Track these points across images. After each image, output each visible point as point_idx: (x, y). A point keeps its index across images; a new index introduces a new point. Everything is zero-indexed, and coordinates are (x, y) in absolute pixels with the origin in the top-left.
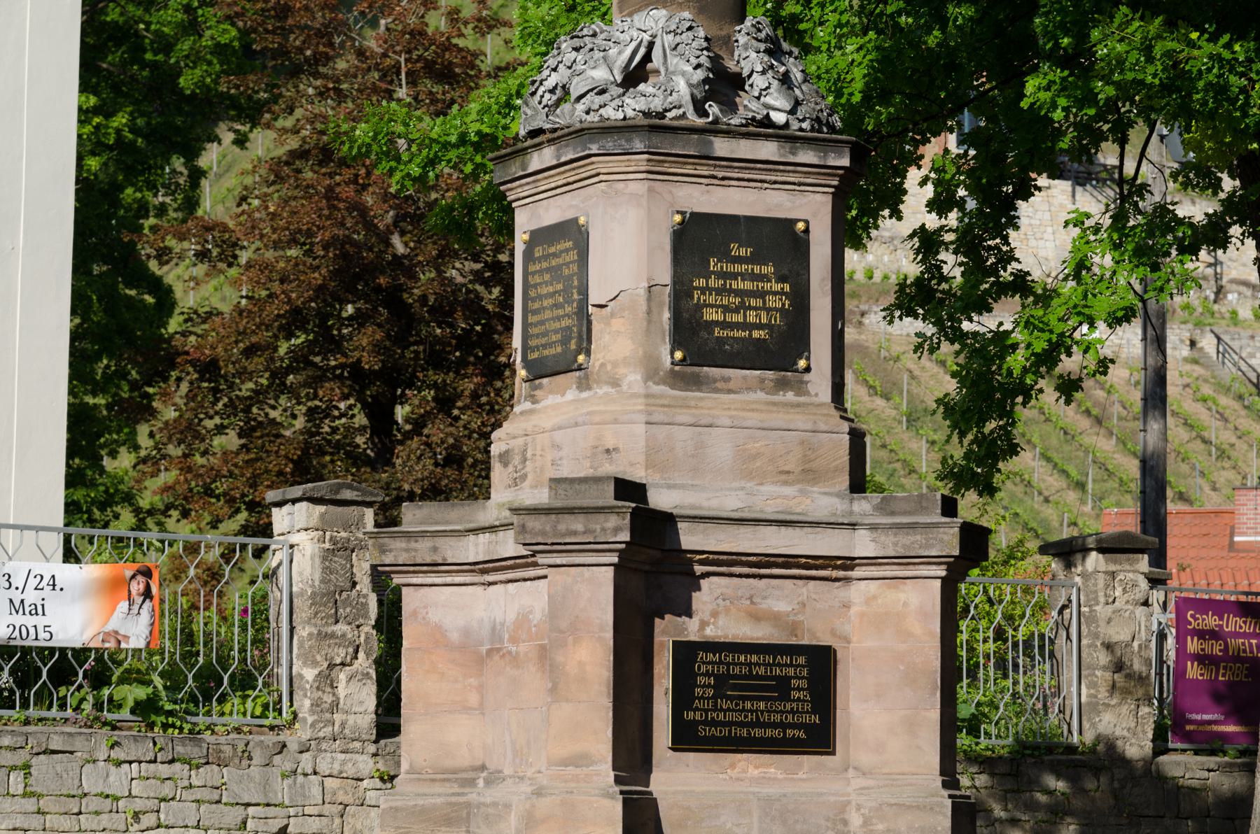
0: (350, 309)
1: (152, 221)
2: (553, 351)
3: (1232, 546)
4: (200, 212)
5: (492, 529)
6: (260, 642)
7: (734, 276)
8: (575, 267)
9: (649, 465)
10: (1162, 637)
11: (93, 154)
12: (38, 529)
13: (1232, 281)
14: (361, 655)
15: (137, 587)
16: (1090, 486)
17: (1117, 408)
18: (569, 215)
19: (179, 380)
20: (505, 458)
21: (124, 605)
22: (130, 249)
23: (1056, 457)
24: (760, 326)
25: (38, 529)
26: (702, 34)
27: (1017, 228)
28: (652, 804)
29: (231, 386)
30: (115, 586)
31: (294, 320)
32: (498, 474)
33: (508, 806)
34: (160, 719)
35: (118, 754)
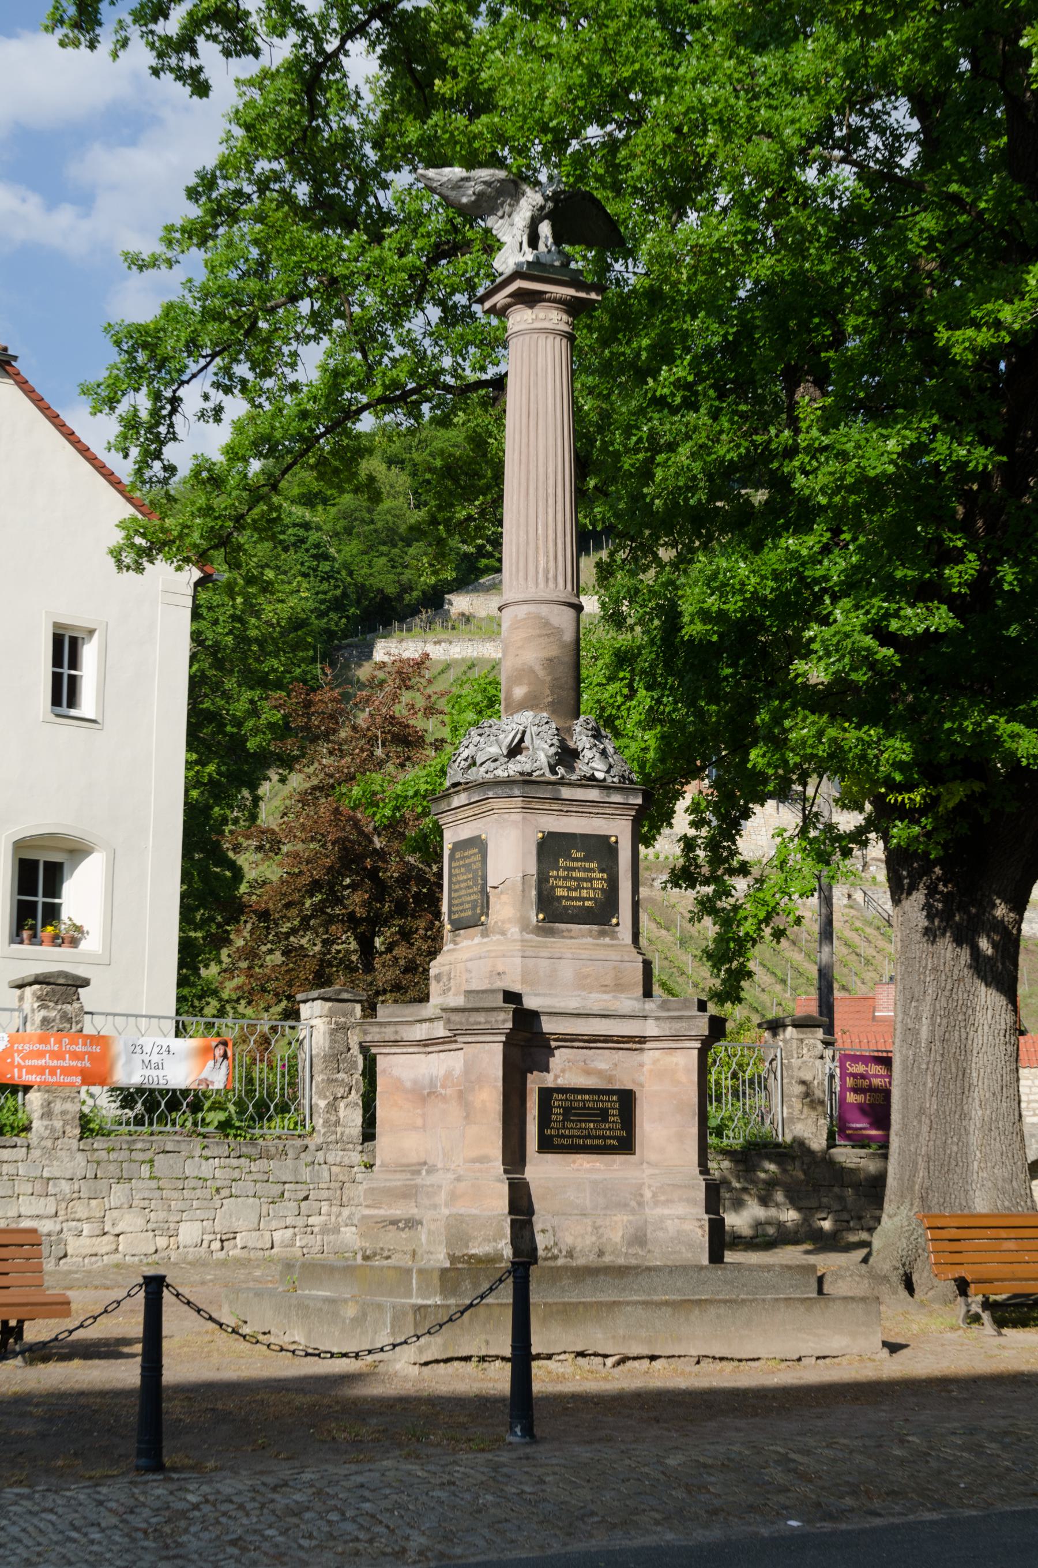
0: (348, 881)
1: (231, 827)
3: (874, 1018)
4: (259, 822)
5: (430, 1020)
6: (292, 1084)
7: (574, 869)
8: (479, 864)
9: (524, 982)
10: (832, 1077)
11: (195, 788)
12: (160, 1017)
13: (873, 859)
14: (353, 1092)
15: (219, 1052)
16: (789, 982)
17: (805, 935)
18: (476, 833)
19: (246, 922)
20: (438, 978)
21: (211, 1063)
22: (217, 845)
23: (768, 964)
24: (589, 899)
25: (160, 1017)
26: (554, 726)
27: (741, 836)
28: (526, 1185)
29: (277, 925)
30: (206, 1052)
31: (315, 886)
32: (434, 988)
33: (440, 1187)
34: (233, 1132)
35: (207, 1153)
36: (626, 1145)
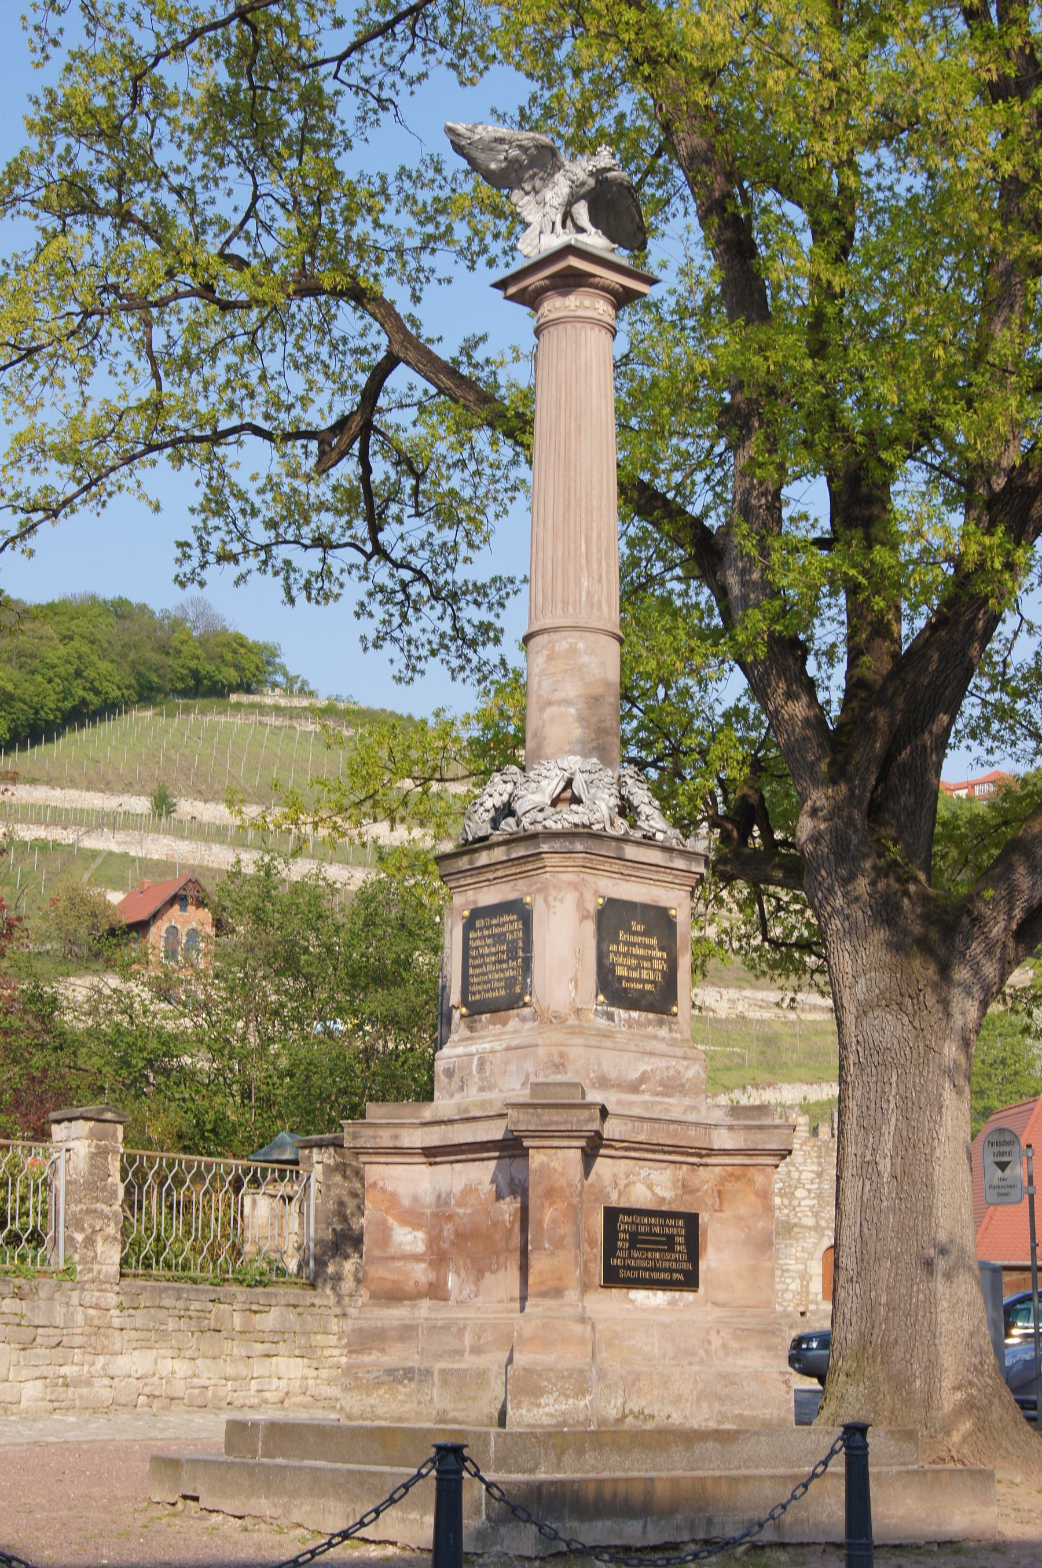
2: (496, 994)
7: (634, 945)
36: (690, 1281)
